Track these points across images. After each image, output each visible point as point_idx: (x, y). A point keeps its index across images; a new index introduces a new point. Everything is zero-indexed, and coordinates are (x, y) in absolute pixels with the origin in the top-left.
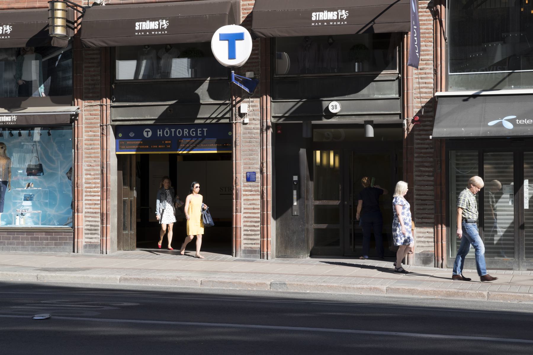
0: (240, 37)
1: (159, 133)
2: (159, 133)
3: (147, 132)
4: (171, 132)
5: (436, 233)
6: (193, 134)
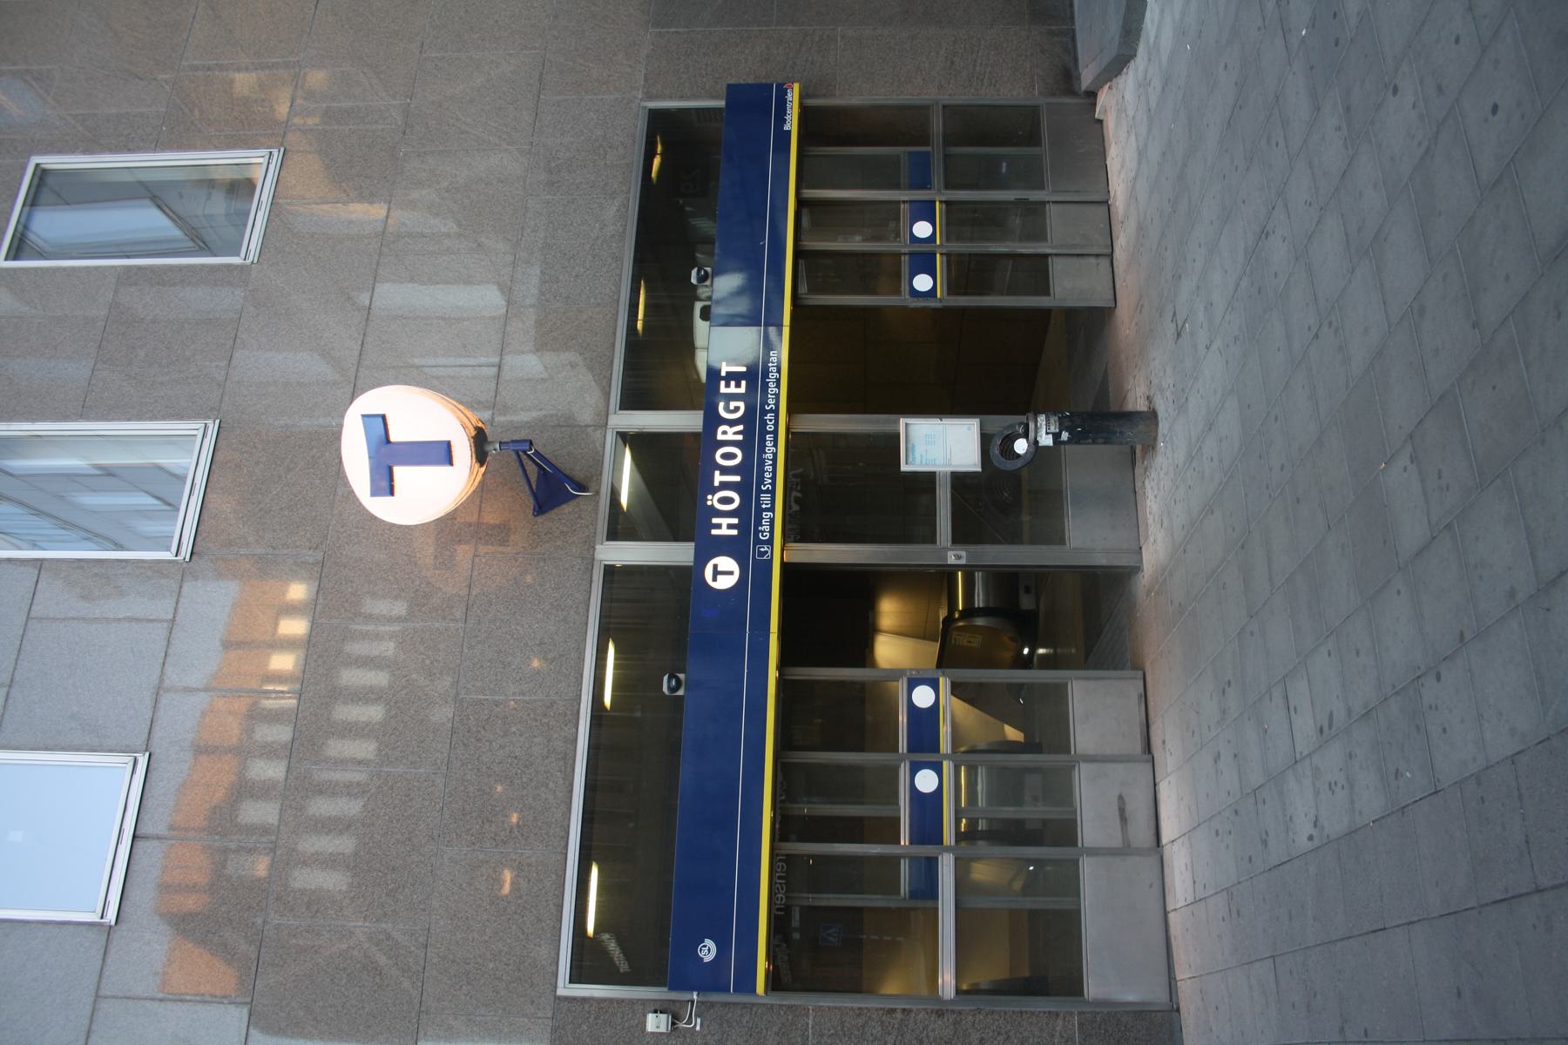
0: (715, 566)
1: (724, 527)
2: (724, 531)
3: (716, 573)
4: (725, 486)
5: (192, 889)
6: (737, 409)
